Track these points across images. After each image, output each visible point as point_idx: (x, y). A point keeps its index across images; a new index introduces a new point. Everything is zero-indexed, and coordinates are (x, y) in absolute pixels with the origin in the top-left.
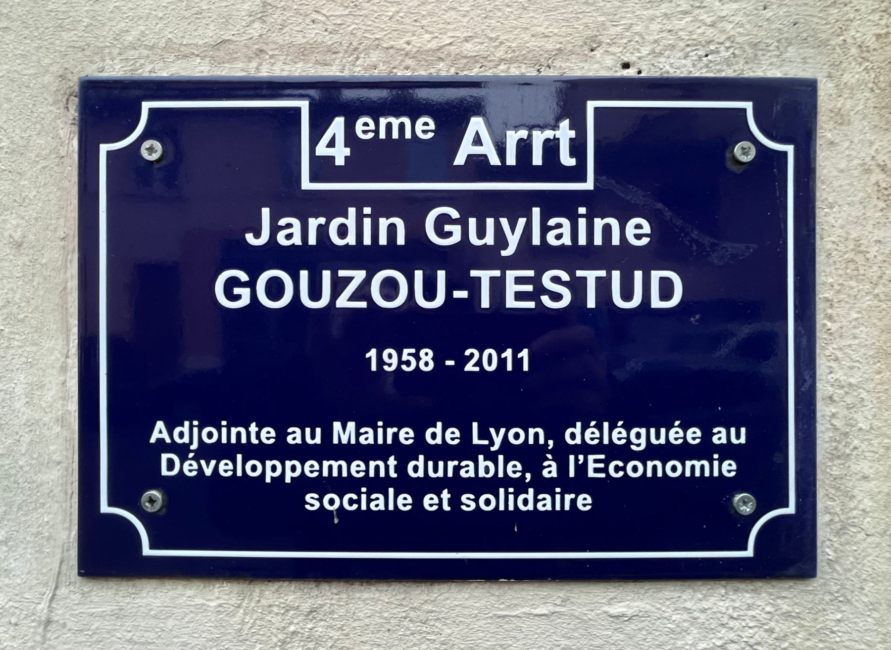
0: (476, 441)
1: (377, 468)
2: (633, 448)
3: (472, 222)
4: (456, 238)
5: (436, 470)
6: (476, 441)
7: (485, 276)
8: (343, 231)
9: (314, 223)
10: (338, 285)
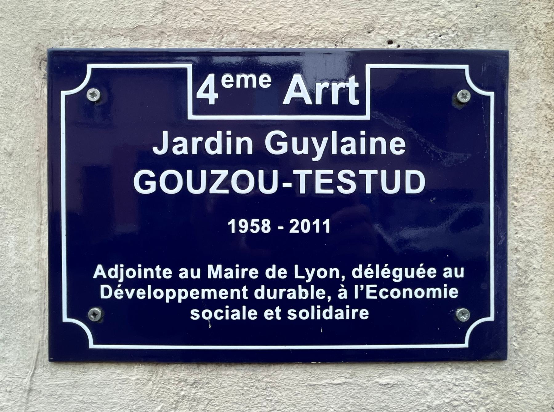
0: (297, 276)
1: (235, 293)
2: (394, 280)
3: (295, 140)
4: (284, 150)
5: (272, 295)
6: (297, 276)
7: (302, 174)
8: (214, 146)
9: (195, 141)
10: (211, 180)
